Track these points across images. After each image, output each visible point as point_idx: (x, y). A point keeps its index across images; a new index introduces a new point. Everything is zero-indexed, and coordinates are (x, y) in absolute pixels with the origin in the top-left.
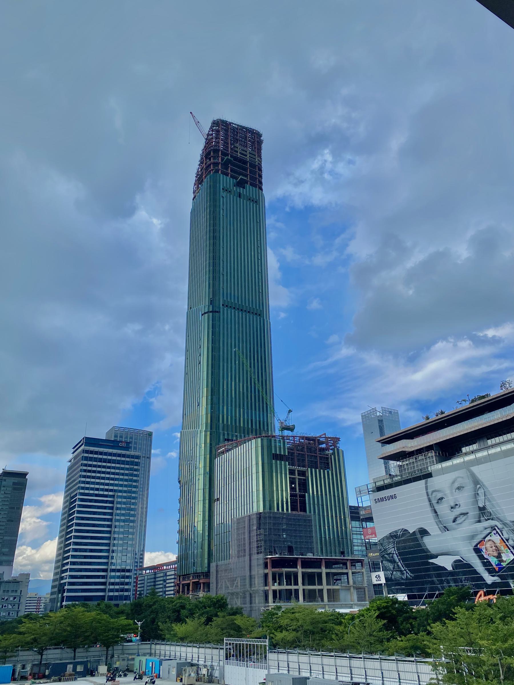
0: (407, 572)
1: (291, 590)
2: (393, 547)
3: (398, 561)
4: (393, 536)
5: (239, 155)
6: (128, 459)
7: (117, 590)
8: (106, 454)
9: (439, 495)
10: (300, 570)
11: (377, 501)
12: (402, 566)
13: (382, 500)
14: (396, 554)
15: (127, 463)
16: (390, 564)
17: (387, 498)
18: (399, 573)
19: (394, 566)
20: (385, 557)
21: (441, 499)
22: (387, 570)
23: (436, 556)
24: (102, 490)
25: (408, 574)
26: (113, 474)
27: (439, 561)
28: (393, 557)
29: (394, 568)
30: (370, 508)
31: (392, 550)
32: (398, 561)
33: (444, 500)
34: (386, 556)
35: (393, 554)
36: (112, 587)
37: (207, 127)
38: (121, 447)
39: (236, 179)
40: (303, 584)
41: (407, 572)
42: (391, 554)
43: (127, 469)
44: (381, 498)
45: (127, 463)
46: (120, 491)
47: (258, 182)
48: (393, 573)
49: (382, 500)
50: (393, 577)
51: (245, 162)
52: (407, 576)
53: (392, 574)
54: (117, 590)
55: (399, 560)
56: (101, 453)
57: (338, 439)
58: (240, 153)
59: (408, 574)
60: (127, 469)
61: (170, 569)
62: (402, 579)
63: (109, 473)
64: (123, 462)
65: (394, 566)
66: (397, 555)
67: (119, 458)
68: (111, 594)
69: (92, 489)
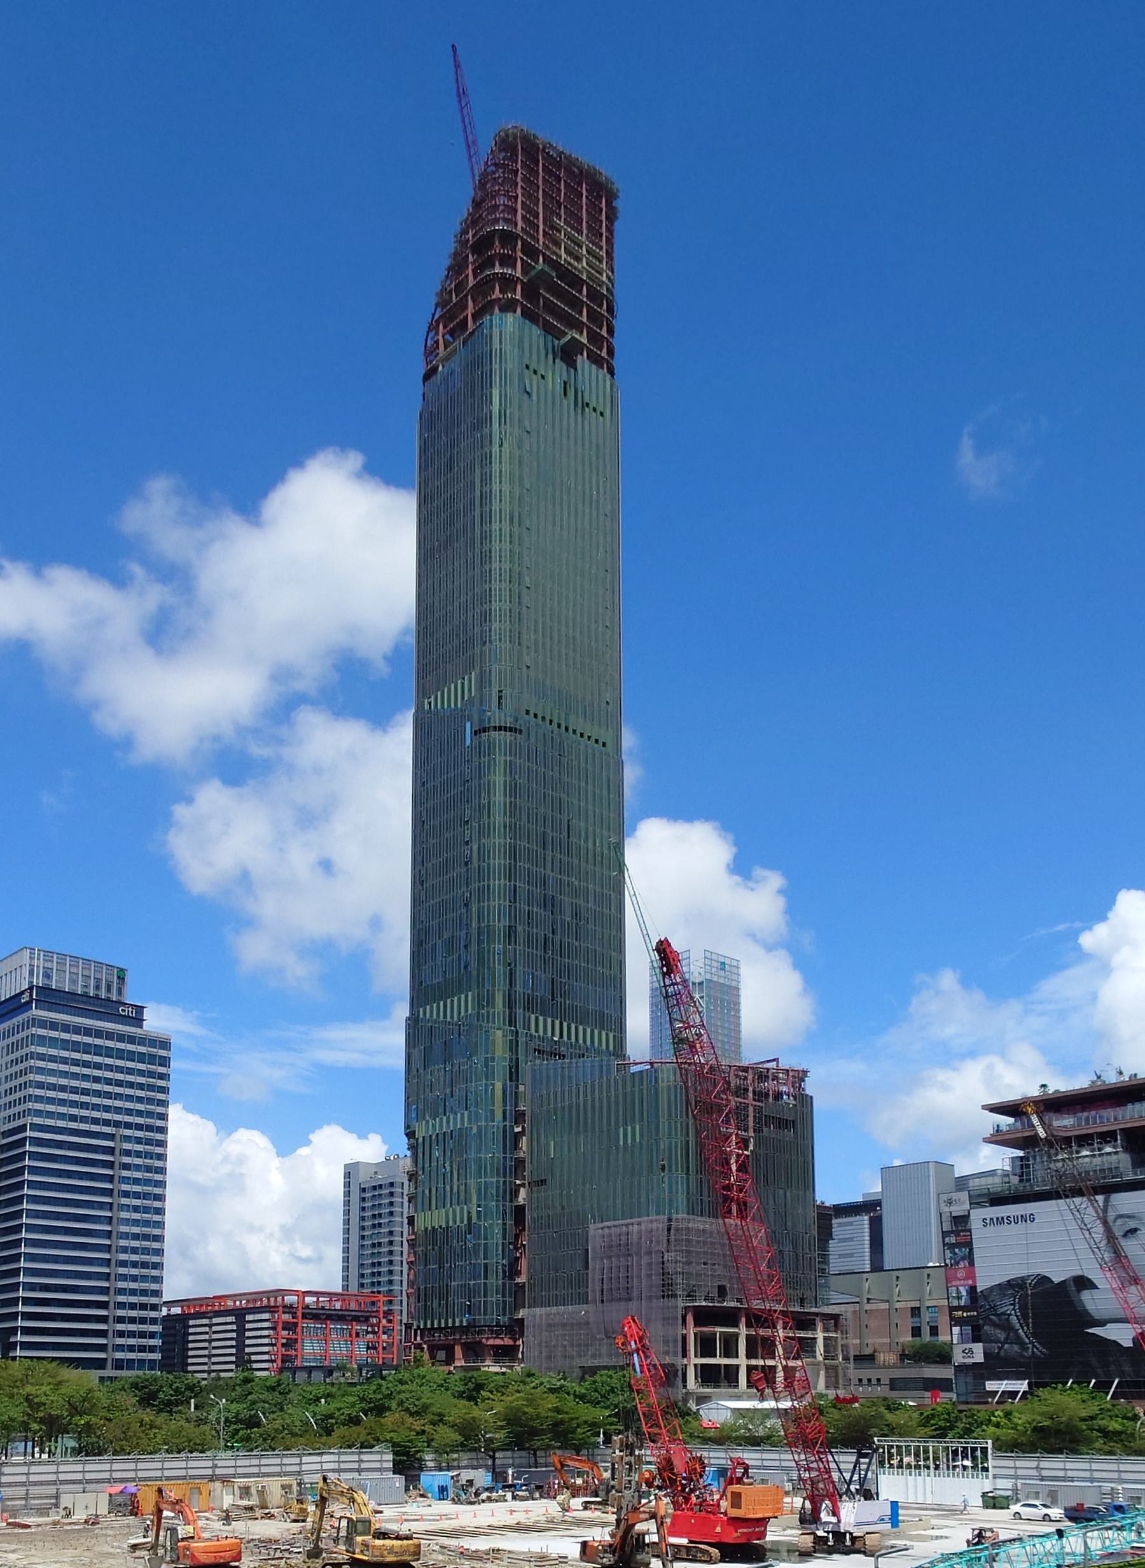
0: (1034, 1346)
1: (719, 1365)
2: (1011, 1304)
3: (1018, 1326)
4: (1015, 1286)
5: (564, 255)
6: (142, 1049)
7: (131, 1349)
8: (110, 1036)
9: (1132, 1224)
10: (743, 1331)
11: (988, 1222)
12: (1027, 1336)
13: (1000, 1221)
14: (1017, 1316)
15: (141, 1058)
16: (999, 1331)
17: (1012, 1220)
18: (1016, 1348)
19: (1009, 1334)
20: (991, 1320)
21: (1133, 1231)
22: (992, 1342)
23: (1102, 1323)
24: (83, 1119)
25: (1035, 1349)
26: (109, 1082)
27: (1111, 1332)
28: (1008, 1320)
29: (1006, 1339)
30: (968, 1233)
31: (1009, 1309)
32: (1018, 1326)
33: (1139, 1232)
34: (993, 1317)
35: (1010, 1315)
36: (120, 1341)
37: (486, 144)
38: (125, 1016)
39: (561, 334)
40: (748, 1357)
41: (1034, 1346)
42: (1006, 1314)
43: (141, 1073)
44: (998, 1219)
45: (141, 1058)
46: (128, 1126)
47: (605, 350)
48: (1003, 1346)
49: (1000, 1221)
50: (1002, 1353)
51: (576, 282)
52: (1033, 1352)
53: (1000, 1348)
54: (131, 1349)
55: (1021, 1325)
56: (99, 1034)
57: (805, 1072)
58: (567, 251)
59: (1035, 1349)
60: (141, 1073)
61: (201, 1306)
62: (1023, 1357)
63: (97, 1080)
64: (131, 1055)
65: (1009, 1334)
66: (1018, 1319)
67: (88, 1040)
68: (119, 1355)
69: (62, 1116)
